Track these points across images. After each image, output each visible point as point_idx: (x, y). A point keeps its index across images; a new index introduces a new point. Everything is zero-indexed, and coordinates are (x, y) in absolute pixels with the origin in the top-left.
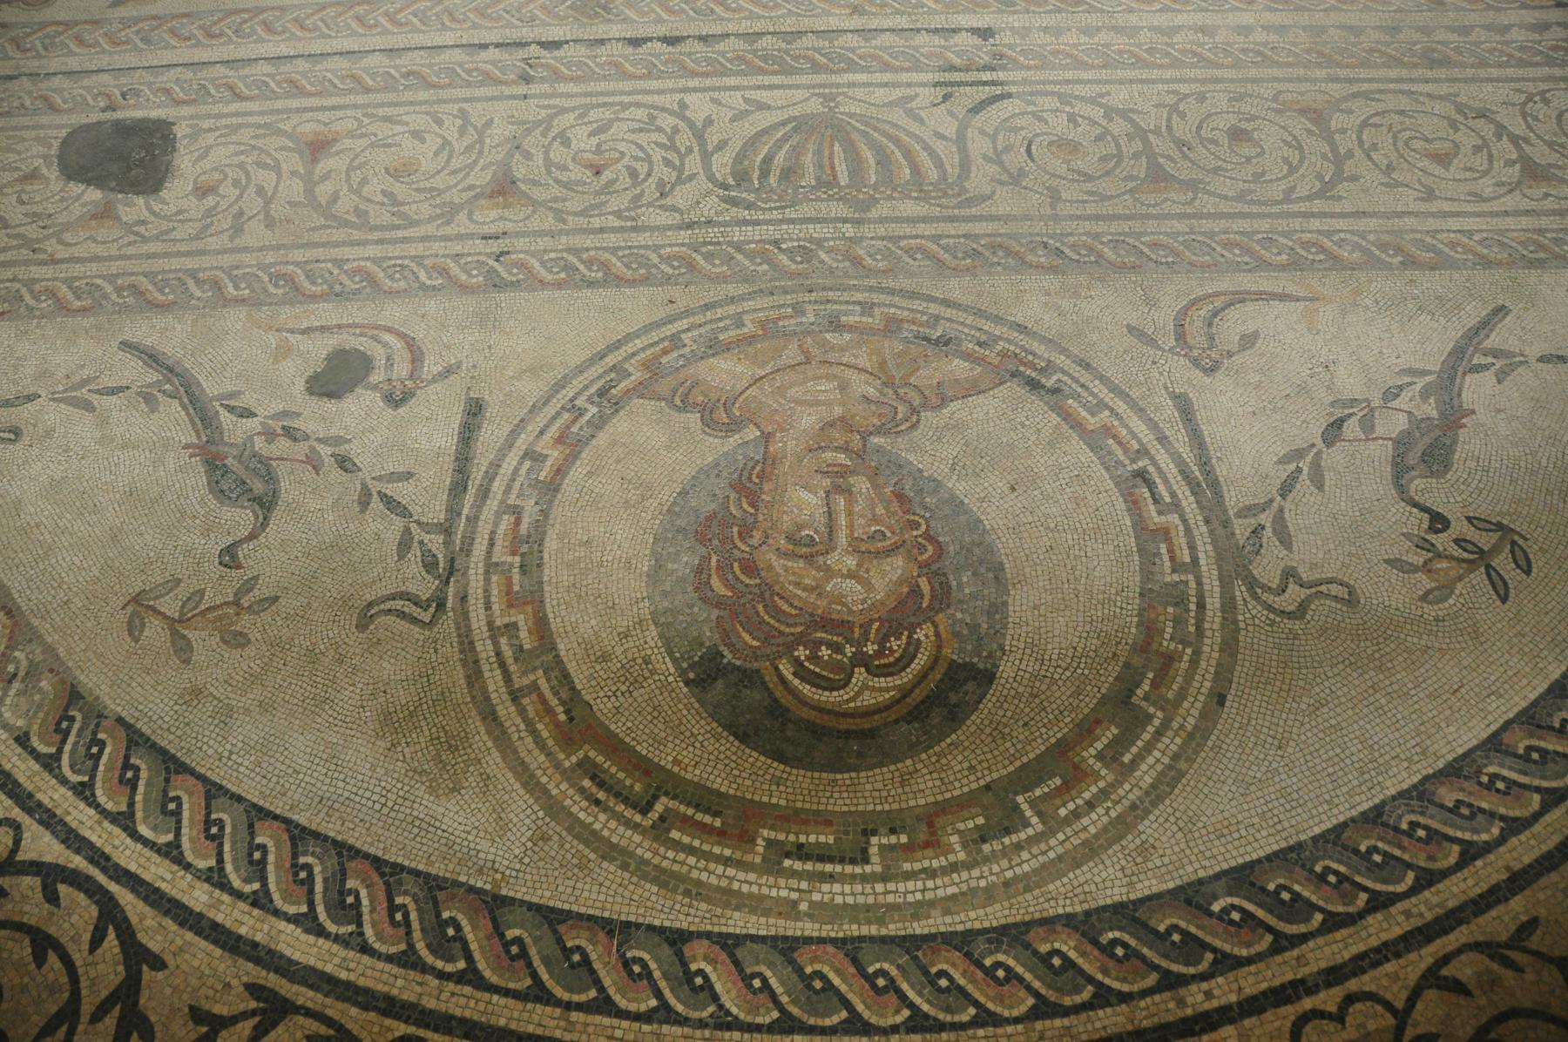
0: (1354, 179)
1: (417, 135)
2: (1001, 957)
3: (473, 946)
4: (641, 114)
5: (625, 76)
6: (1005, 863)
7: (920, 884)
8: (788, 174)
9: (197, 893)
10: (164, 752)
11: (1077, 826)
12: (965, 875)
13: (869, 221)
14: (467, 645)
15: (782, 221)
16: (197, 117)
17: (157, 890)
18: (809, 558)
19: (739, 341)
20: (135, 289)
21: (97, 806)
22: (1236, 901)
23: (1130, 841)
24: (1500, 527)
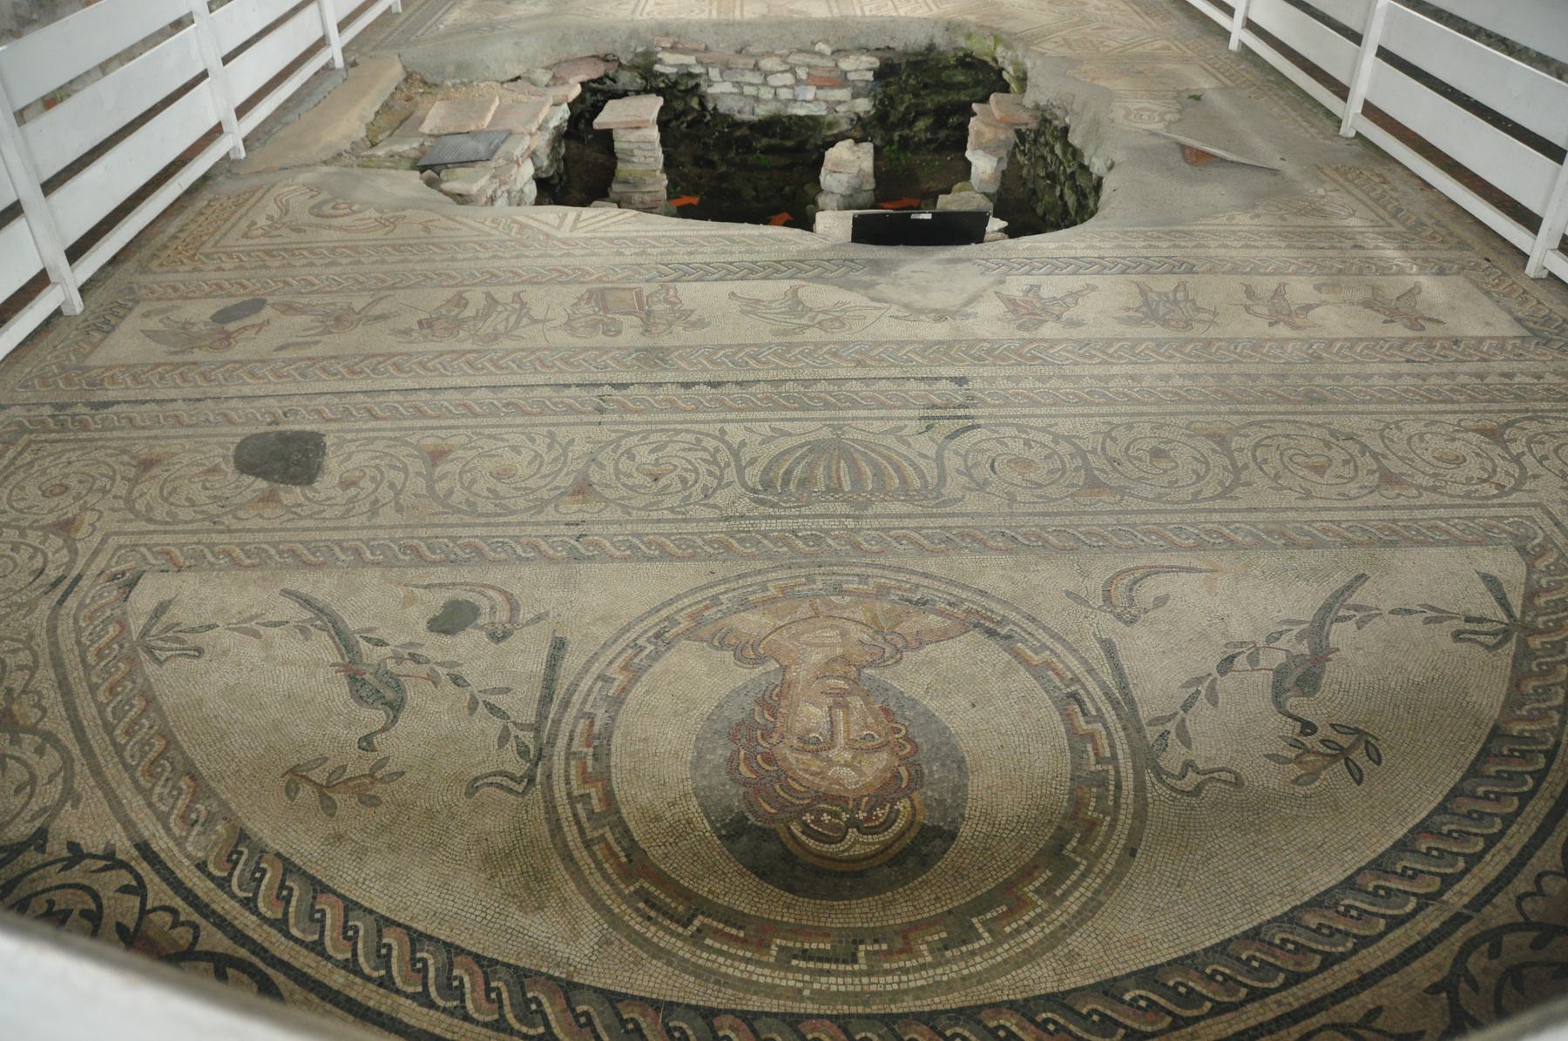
0: (1248, 484)
1: (515, 449)
2: (959, 1030)
3: (551, 1018)
4: (690, 437)
5: (677, 409)
6: (962, 964)
7: (896, 979)
8: (803, 483)
9: (336, 977)
10: (312, 879)
11: (1019, 939)
12: (931, 972)
13: (866, 517)
14: (551, 807)
15: (799, 516)
16: (342, 430)
17: (304, 974)
18: (815, 753)
19: (764, 602)
20: (292, 552)
21: (259, 914)
22: (1143, 993)
23: (1060, 951)
24: (1357, 730)
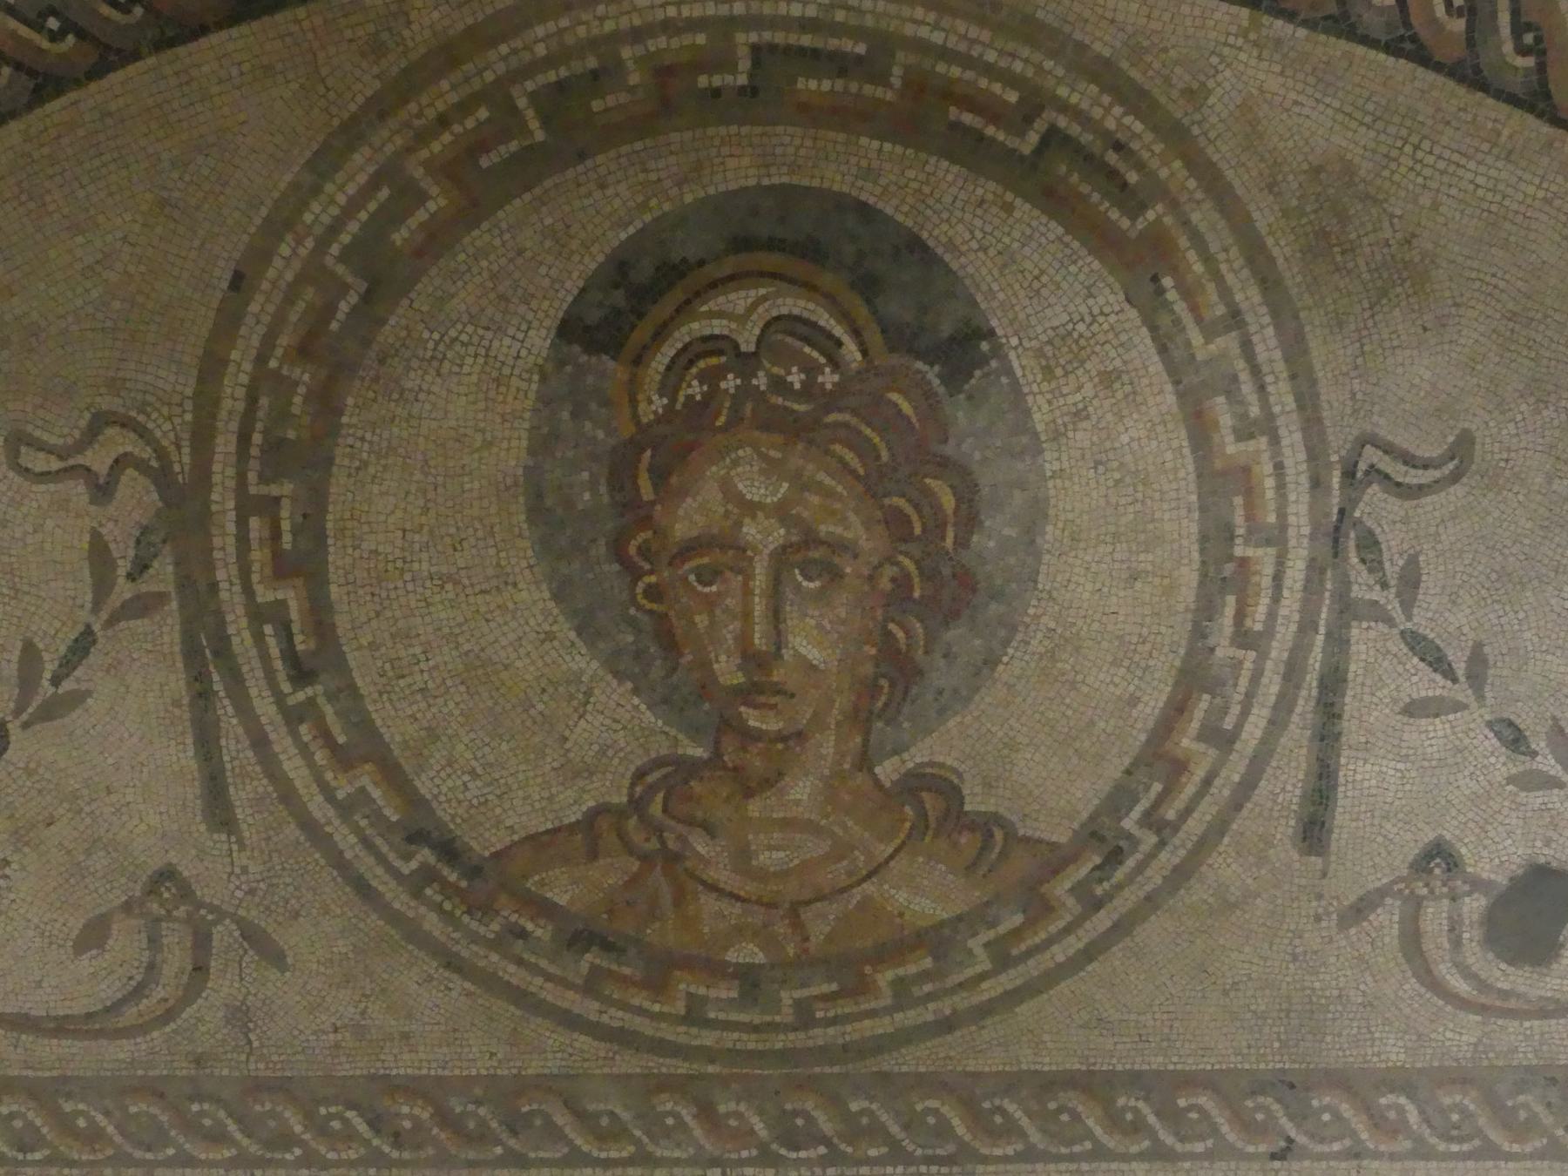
18: (811, 539)
